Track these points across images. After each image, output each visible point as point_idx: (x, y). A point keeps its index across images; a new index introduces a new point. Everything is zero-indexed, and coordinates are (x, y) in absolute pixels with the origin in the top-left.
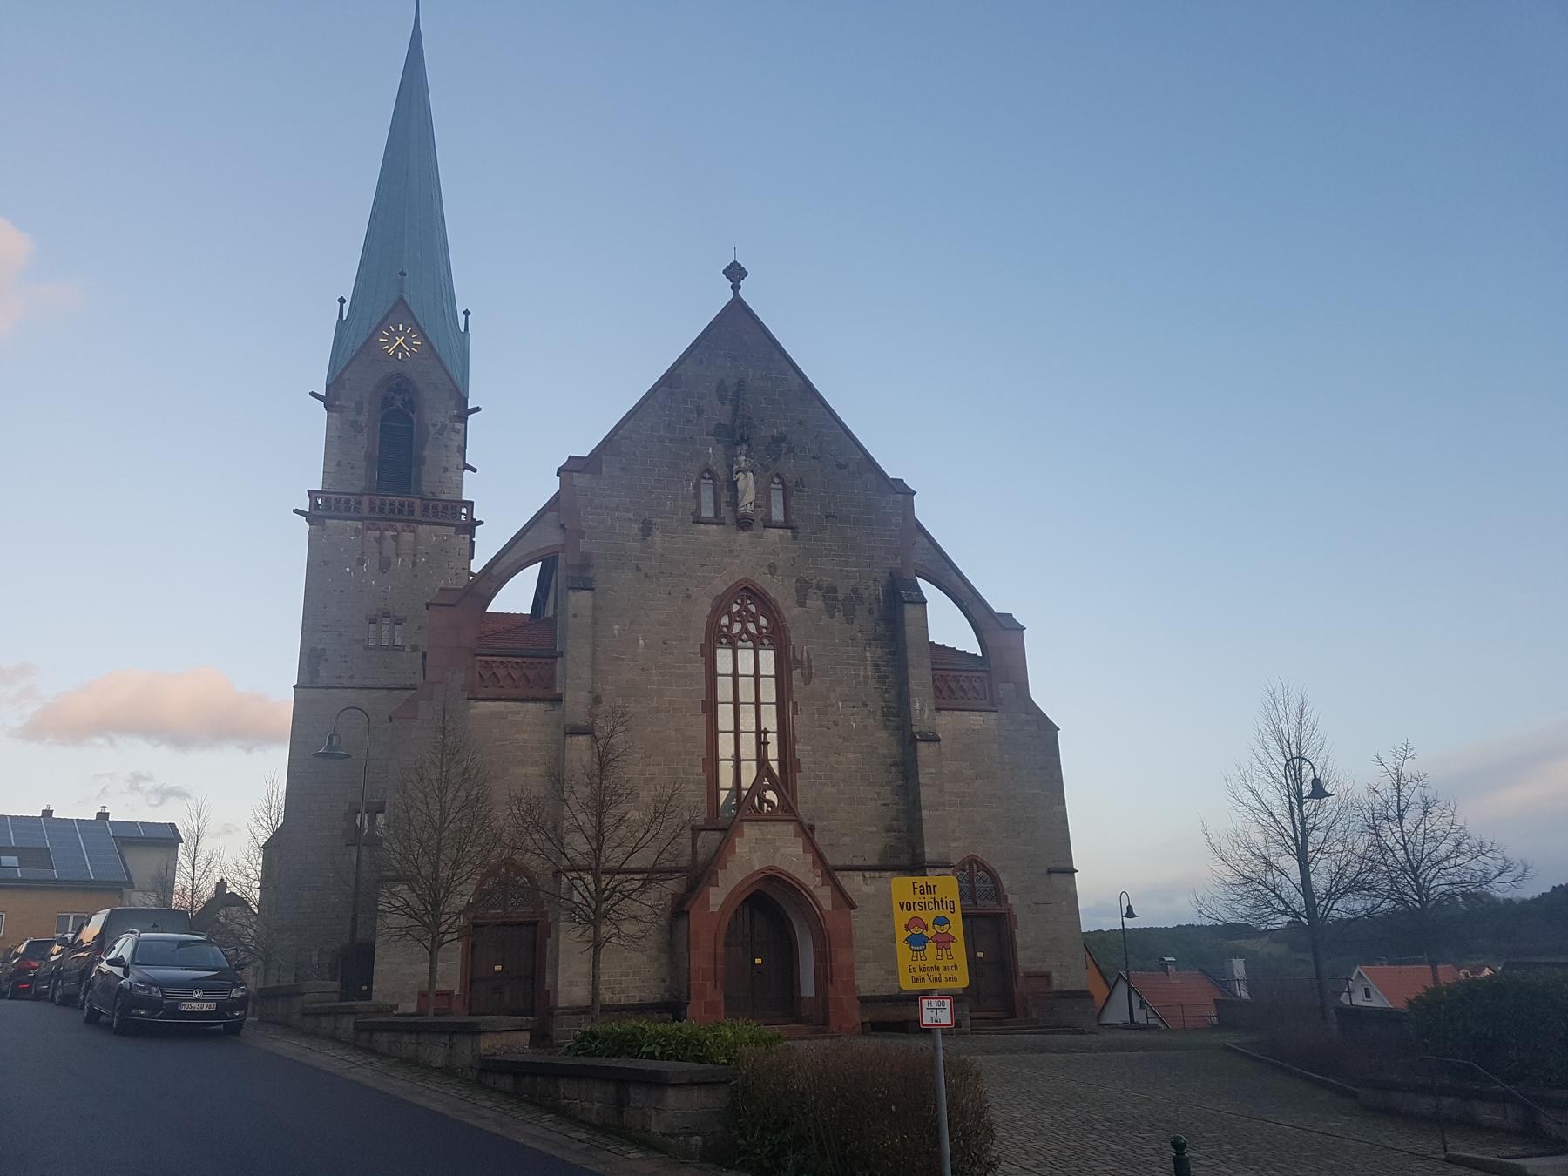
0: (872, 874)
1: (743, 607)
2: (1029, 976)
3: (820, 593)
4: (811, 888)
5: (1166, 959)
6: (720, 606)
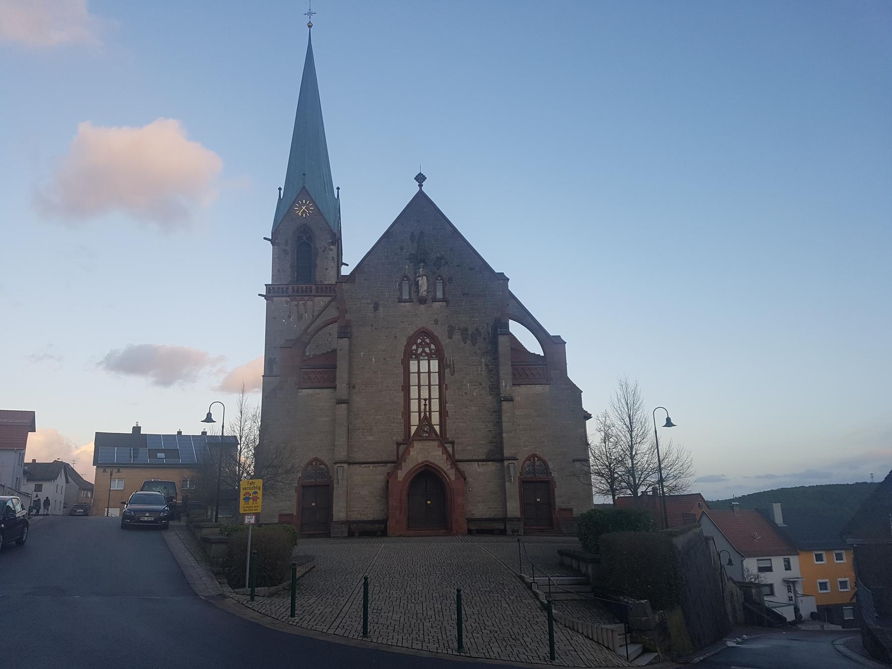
0: (482, 463)
1: (423, 340)
2: (561, 510)
3: (460, 332)
4: (445, 470)
5: (733, 503)
6: (411, 340)
